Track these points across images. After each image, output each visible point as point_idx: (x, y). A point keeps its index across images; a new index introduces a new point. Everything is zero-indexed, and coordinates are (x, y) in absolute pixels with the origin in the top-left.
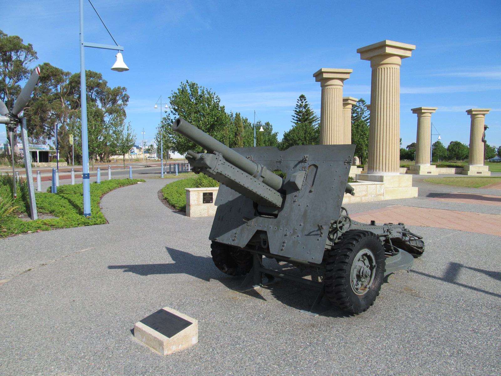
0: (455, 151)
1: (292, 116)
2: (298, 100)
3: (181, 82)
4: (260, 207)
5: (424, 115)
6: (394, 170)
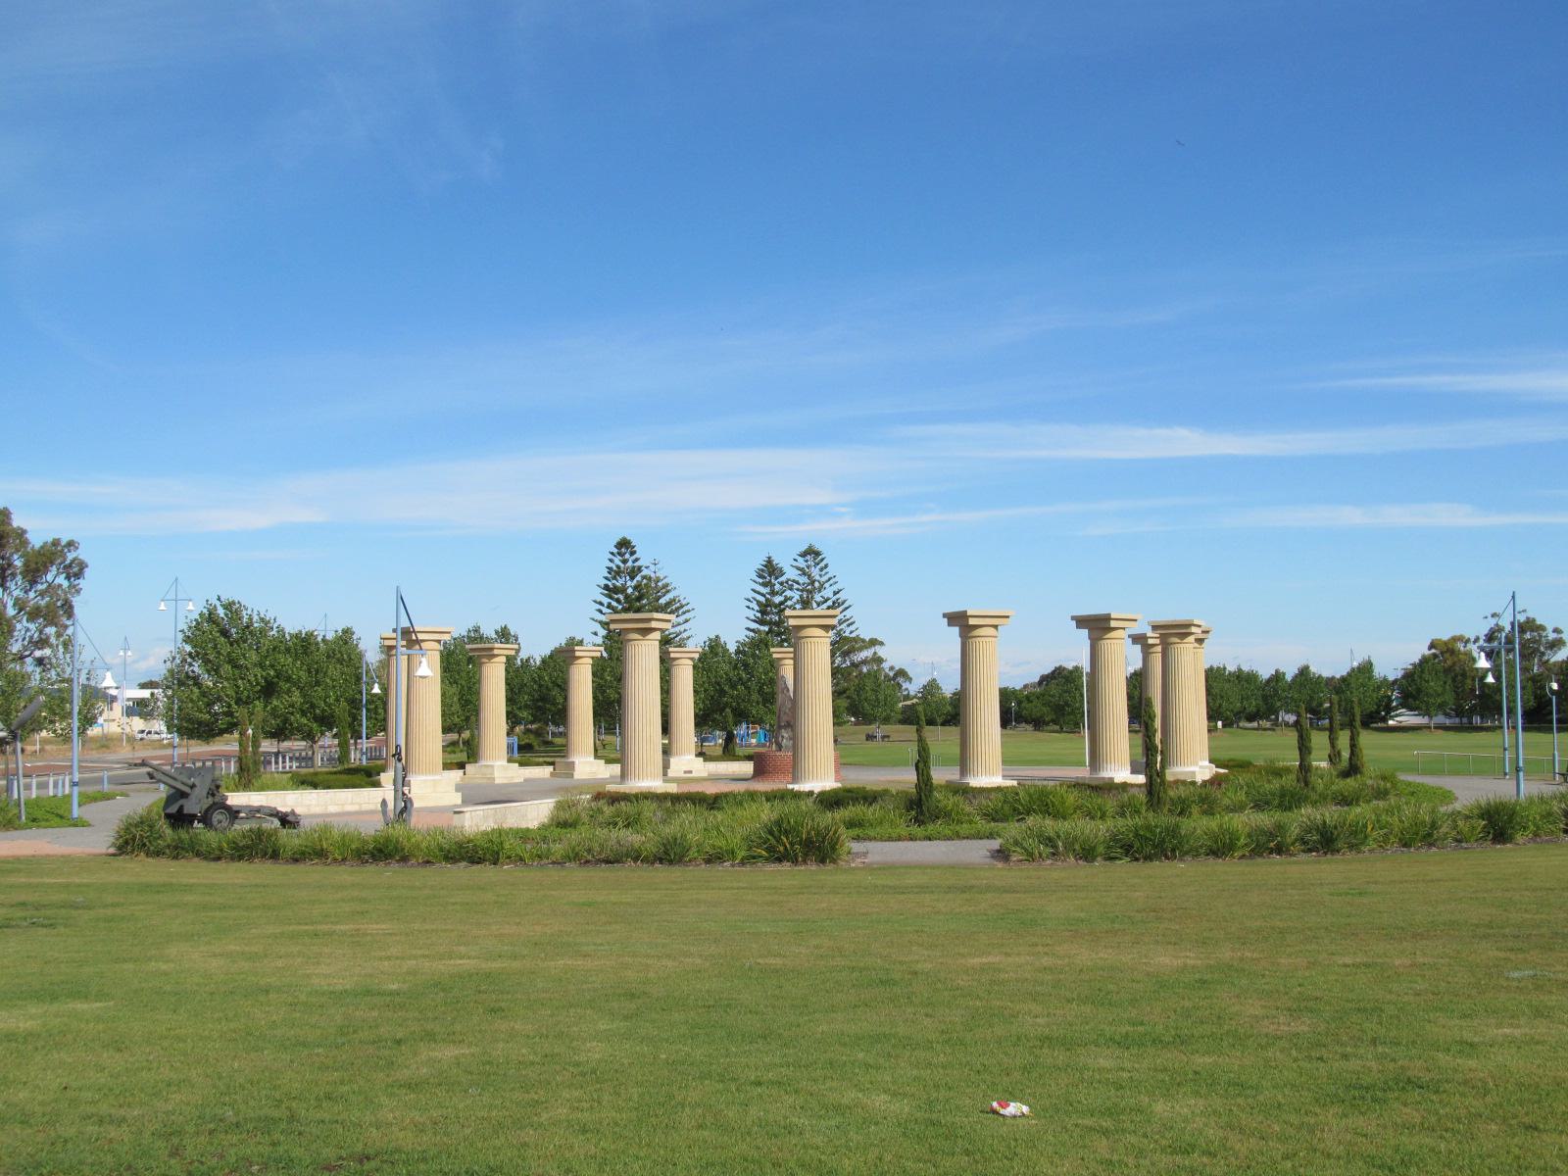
1: (595, 601)
2: (612, 553)
3: (207, 601)
4: (184, 795)
5: (675, 663)
6: (431, 772)
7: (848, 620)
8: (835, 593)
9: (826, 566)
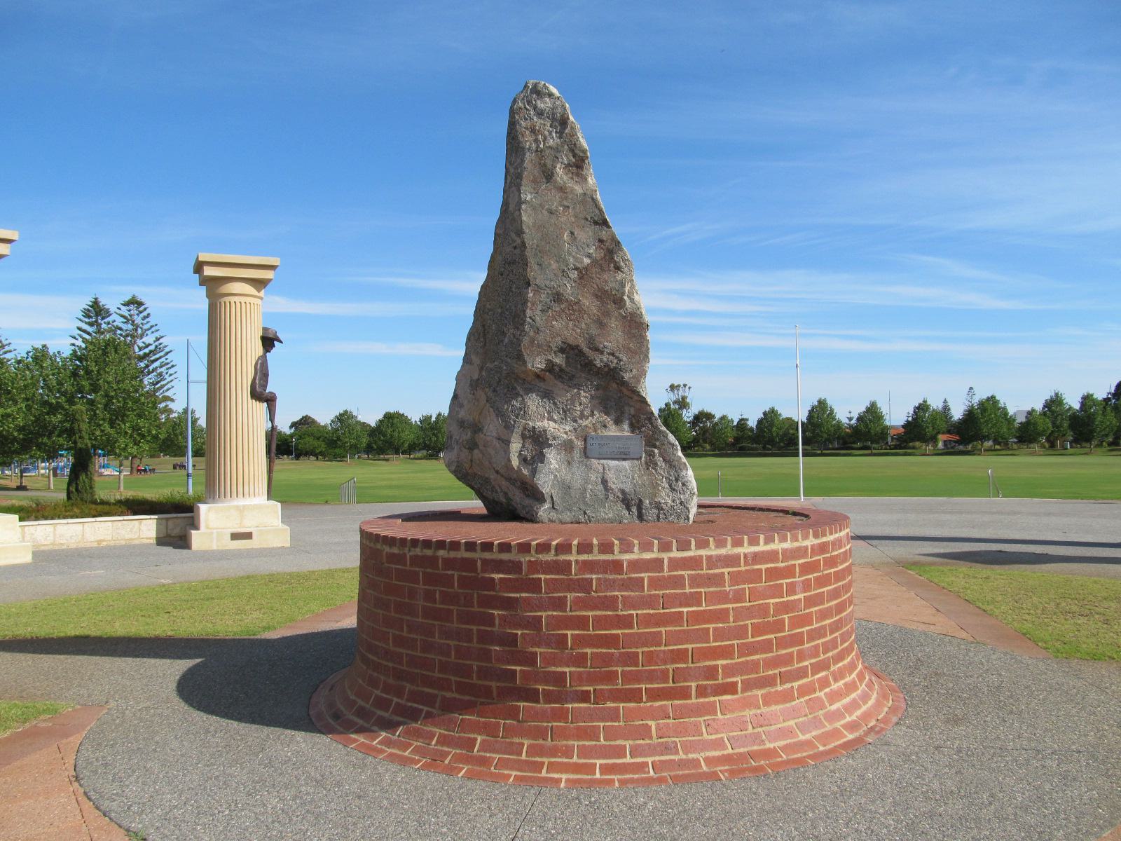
0: (384, 435)
7: (168, 364)
8: (158, 339)
9: (148, 315)
